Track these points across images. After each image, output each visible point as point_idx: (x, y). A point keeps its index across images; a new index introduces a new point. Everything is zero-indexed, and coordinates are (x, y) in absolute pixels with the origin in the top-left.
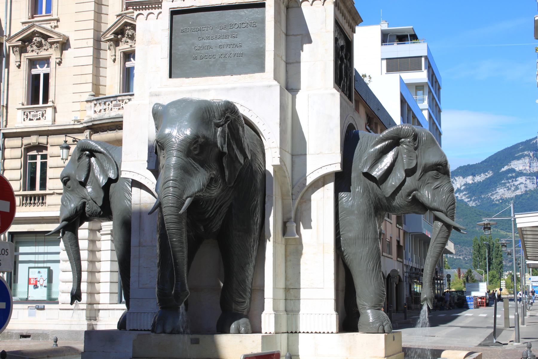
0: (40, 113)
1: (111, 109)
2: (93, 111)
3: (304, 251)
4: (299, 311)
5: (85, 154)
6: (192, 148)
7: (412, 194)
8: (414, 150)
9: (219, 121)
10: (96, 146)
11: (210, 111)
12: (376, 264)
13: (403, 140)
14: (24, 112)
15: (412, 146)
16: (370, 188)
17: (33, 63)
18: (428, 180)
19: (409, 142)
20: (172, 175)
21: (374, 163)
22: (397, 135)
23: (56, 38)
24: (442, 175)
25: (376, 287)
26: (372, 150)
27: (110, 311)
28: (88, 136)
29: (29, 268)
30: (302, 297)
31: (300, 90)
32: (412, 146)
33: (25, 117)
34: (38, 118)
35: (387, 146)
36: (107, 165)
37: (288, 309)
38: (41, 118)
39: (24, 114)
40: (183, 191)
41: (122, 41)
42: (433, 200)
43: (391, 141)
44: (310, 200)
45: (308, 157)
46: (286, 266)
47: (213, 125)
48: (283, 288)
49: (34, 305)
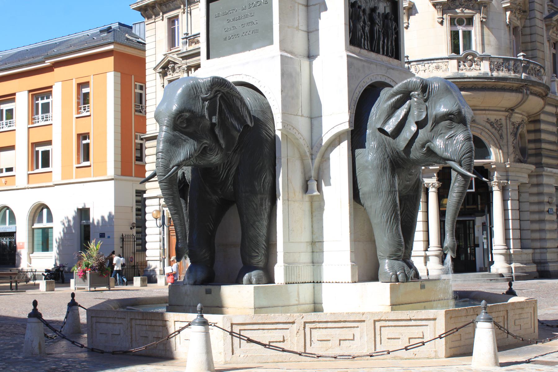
4: (323, 262)
6: (178, 122)
7: (426, 146)
8: (423, 102)
9: (206, 96)
11: (197, 87)
12: (390, 216)
13: (413, 93)
15: (421, 98)
16: (385, 142)
18: (441, 131)
19: (418, 95)
21: (387, 118)
22: (406, 89)
24: (456, 124)
25: (390, 239)
30: (325, 249)
31: (318, 57)
32: (421, 98)
37: (315, 261)
43: (402, 95)
44: (329, 159)
46: (312, 222)
47: (201, 100)
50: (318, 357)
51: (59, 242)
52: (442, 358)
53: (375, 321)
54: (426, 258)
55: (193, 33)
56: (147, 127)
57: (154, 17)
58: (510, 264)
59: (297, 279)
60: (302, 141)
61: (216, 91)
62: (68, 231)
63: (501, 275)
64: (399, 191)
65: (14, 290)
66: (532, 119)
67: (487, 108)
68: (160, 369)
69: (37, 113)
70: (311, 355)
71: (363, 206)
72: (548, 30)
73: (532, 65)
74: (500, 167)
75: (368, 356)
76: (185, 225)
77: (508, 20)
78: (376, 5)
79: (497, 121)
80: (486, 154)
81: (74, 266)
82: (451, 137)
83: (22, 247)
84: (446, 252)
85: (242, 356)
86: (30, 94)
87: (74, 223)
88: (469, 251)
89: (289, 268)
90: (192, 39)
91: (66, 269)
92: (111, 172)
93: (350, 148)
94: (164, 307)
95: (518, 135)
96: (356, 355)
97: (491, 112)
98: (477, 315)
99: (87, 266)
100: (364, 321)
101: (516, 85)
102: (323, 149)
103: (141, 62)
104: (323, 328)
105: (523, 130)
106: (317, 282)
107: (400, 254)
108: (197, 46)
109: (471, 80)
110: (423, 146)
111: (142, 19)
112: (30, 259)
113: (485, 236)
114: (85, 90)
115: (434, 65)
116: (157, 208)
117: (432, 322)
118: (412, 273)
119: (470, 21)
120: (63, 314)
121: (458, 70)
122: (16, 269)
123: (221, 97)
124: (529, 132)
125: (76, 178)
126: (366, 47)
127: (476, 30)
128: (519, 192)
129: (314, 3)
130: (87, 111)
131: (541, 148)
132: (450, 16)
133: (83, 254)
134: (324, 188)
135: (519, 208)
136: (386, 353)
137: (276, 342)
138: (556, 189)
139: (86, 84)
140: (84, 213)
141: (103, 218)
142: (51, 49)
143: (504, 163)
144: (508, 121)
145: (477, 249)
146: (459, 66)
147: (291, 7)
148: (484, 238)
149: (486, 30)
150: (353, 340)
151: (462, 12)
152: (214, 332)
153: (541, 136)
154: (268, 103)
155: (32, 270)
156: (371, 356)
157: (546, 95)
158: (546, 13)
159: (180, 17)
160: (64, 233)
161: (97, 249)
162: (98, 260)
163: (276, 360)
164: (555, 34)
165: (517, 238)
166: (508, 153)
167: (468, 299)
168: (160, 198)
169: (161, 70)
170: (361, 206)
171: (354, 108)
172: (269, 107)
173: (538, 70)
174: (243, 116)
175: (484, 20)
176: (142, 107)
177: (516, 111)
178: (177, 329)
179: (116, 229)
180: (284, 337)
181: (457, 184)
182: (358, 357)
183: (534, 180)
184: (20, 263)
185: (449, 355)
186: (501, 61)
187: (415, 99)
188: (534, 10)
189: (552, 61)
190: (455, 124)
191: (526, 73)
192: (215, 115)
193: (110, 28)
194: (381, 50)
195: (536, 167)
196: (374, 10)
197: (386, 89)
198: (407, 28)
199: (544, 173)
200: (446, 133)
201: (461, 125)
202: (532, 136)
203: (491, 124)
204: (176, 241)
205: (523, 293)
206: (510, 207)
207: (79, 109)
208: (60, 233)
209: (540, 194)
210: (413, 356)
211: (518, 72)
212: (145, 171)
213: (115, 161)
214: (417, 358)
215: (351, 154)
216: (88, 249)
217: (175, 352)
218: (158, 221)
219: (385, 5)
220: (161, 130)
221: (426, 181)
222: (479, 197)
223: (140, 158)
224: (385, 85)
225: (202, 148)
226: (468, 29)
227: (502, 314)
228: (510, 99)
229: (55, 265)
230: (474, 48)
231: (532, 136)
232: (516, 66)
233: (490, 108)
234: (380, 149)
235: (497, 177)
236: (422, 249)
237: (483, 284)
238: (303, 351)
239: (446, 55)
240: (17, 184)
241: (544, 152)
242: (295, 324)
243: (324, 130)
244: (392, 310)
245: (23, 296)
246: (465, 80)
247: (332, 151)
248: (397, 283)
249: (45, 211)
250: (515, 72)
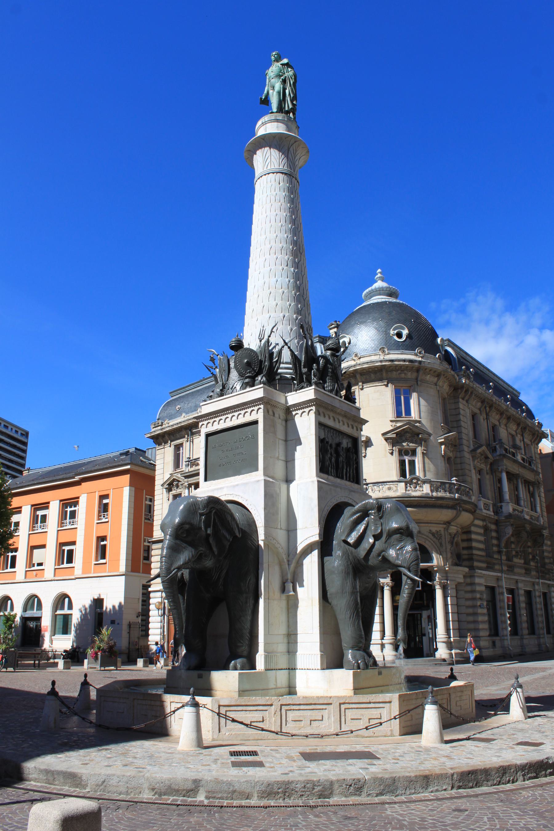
3: (300, 604)
4: (297, 652)
6: (180, 533)
8: (379, 519)
13: (370, 511)
16: (348, 551)
18: (393, 542)
19: (375, 513)
24: (405, 537)
26: (348, 522)
35: (358, 517)
40: (171, 565)
42: (397, 558)
44: (302, 564)
45: (298, 531)
46: (288, 617)
47: (198, 515)
48: (284, 634)
50: (292, 736)
51: (77, 627)
52: (396, 736)
53: (340, 704)
54: (383, 646)
55: (194, 458)
56: (154, 532)
58: (451, 650)
59: (275, 666)
60: (280, 550)
61: (212, 508)
62: (84, 617)
63: (444, 660)
64: (360, 592)
65: (36, 668)
66: (465, 530)
67: (429, 522)
68: (156, 745)
69: (66, 519)
70: (287, 734)
71: (330, 604)
72: (474, 460)
73: (463, 488)
74: (441, 570)
75: (334, 734)
76: (182, 618)
77: (443, 452)
78: (340, 441)
79: (437, 532)
80: (430, 559)
81: (88, 648)
82: (401, 548)
83: (46, 631)
84: (398, 644)
85: (227, 734)
86: (61, 503)
87: (90, 611)
88: (417, 639)
89: (268, 657)
90: (193, 462)
91: (81, 650)
92: (122, 568)
93: (320, 556)
94: (161, 688)
95: (454, 543)
96: (324, 734)
97: (432, 525)
98: (426, 698)
99: (99, 648)
100: (331, 704)
101: (451, 503)
102: (297, 556)
103: (151, 480)
104: (296, 710)
105: (458, 539)
106: (292, 669)
107: (361, 645)
108: (197, 468)
109: (416, 499)
110: (379, 555)
111: (154, 445)
112: (51, 641)
113: (430, 627)
114: (105, 501)
115: (387, 486)
116: (160, 600)
117: (388, 704)
118: (371, 661)
119: (414, 453)
120: (77, 691)
121: (406, 490)
122: (39, 648)
123: (215, 512)
124: (463, 540)
125: (94, 573)
126: (333, 474)
128: (456, 590)
129: (291, 439)
130: (106, 518)
131: (472, 554)
132: (399, 448)
133: (96, 638)
134: (299, 589)
135: (457, 603)
136: (350, 732)
137: (257, 722)
138: (486, 587)
139: (107, 496)
140: (98, 602)
141: (114, 607)
142: (80, 467)
143: (444, 566)
144: (446, 532)
145: (424, 638)
146: (406, 488)
147: (273, 441)
148: (430, 629)
149: (427, 460)
150: (322, 720)
151: (408, 445)
152: (204, 712)
153: (472, 544)
154: (253, 518)
155: (52, 650)
156: (337, 735)
157: (475, 511)
158: (472, 447)
159: (184, 444)
160: (81, 619)
161: (108, 635)
162: (109, 643)
163: (256, 738)
164: (479, 464)
165: (456, 628)
166: (447, 558)
167: (417, 683)
168: (162, 592)
169: (167, 486)
170: (328, 604)
171: (323, 523)
172: (254, 522)
173: (468, 492)
174: (233, 528)
175: (425, 452)
176: (150, 515)
177: (452, 524)
178: (173, 709)
179: (125, 616)
180: (263, 718)
181: (407, 587)
182: (326, 735)
183: (468, 580)
184: (43, 643)
185: (402, 733)
186: (439, 484)
187: (372, 517)
188: (465, 475)
189: (478, 484)
190: (404, 537)
191: (458, 494)
192: (210, 527)
193: (128, 451)
194: (345, 477)
195: (469, 570)
196: (338, 445)
197: (349, 508)
198: (365, 457)
199: (475, 574)
200: (397, 545)
201: (409, 538)
202: (465, 544)
203: (433, 534)
204: (174, 632)
205: (462, 675)
206: (449, 603)
207: (99, 516)
208: (78, 619)
209: (473, 591)
210: (372, 734)
211: (452, 493)
212: (151, 569)
213: (127, 560)
214: (376, 737)
215: (320, 561)
216: (100, 634)
217: (170, 729)
218: (160, 611)
219: (348, 441)
220: (165, 536)
221: (382, 580)
222: (425, 594)
223: (148, 558)
224: (347, 505)
225: (199, 554)
226: (413, 458)
227: (446, 696)
228: (446, 514)
229: (72, 646)
230: (417, 474)
231: (465, 544)
232: (450, 488)
233: (432, 522)
234: (344, 557)
235: (438, 578)
236: (379, 638)
237: (430, 667)
238: (280, 731)
239: (395, 478)
240: (45, 577)
241: (475, 557)
242: (273, 706)
243: (299, 541)
244: (354, 694)
245: (44, 673)
246: (412, 499)
247: (305, 558)
248: (359, 670)
249: (67, 600)
250: (450, 493)
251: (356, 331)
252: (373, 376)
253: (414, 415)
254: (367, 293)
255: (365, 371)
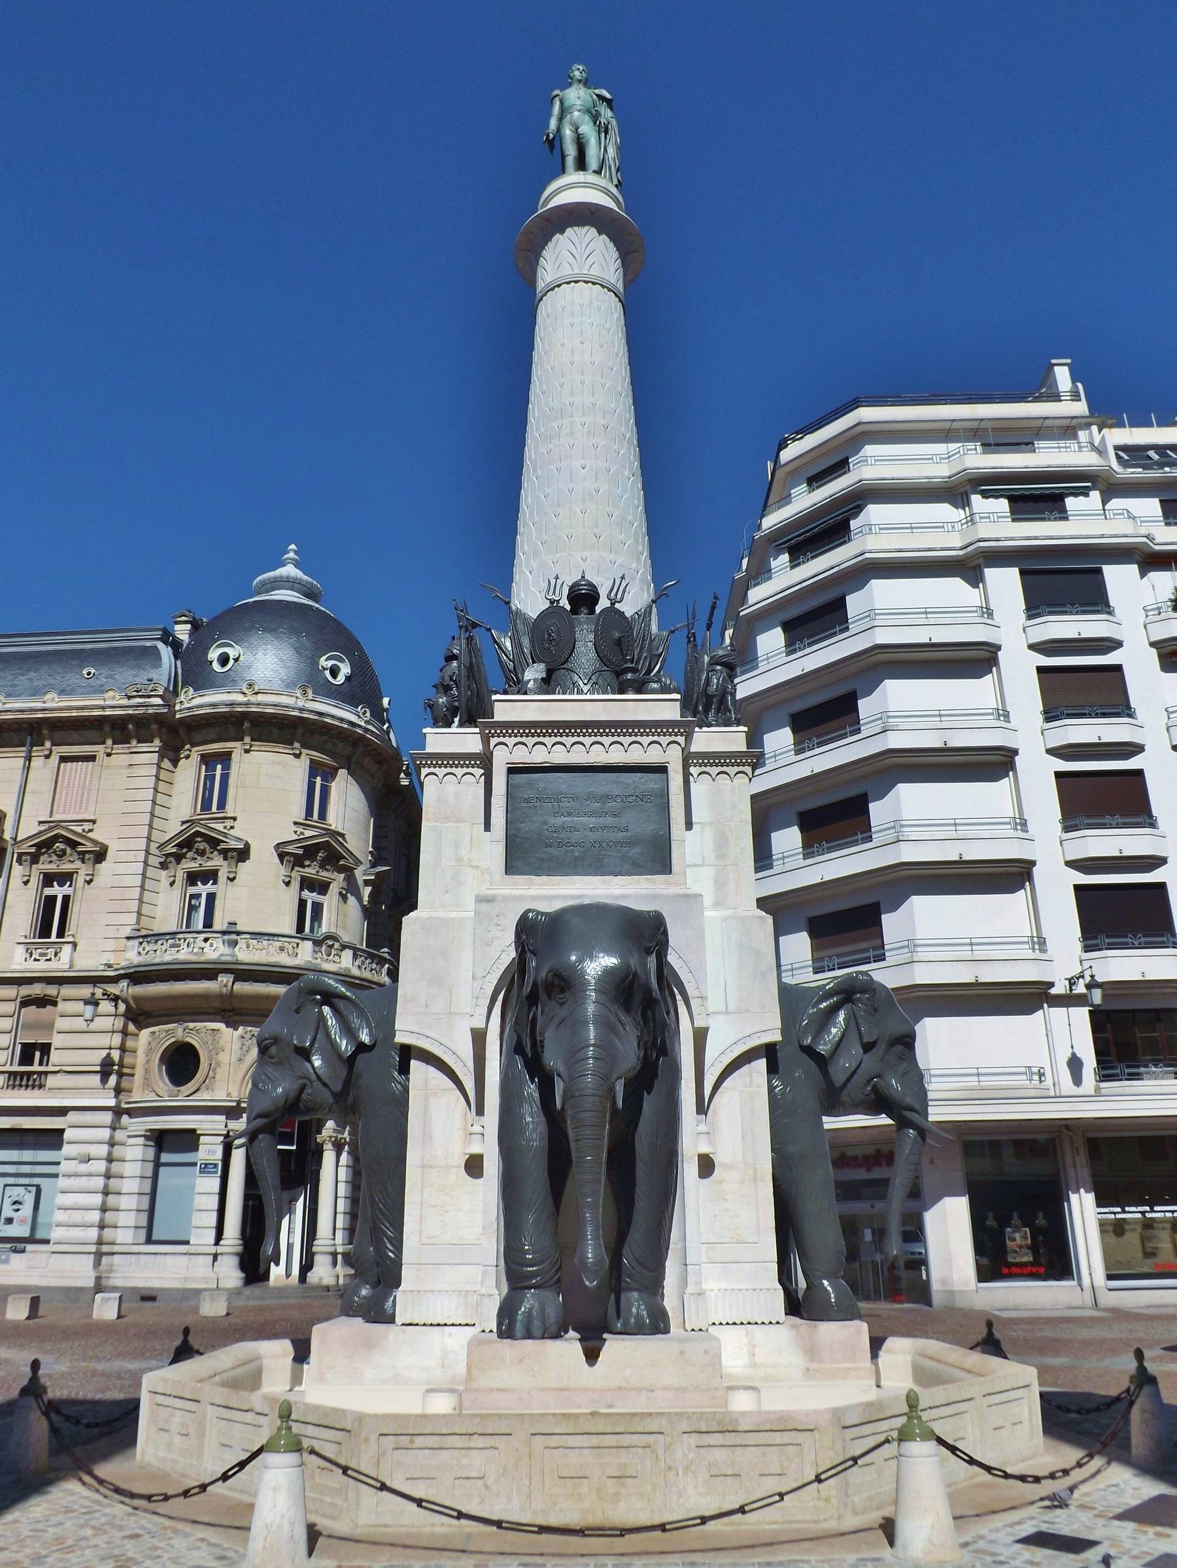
0: (51, 951)
1: (166, 950)
2: (135, 952)
5: (314, 999)
7: (872, 1083)
10: (337, 987)
14: (28, 949)
17: (49, 879)
20: (592, 1035)
23: (90, 847)
27: (133, 1256)
28: (125, 987)
29: (6, 1186)
33: (28, 955)
34: (48, 958)
36: (356, 1020)
38: (53, 958)
39: (27, 951)
41: (187, 856)
49: (9, 1246)
57: (109, 742)
115: (278, 944)
127: (329, 902)
136: (350, 1472)
175: (344, 892)
251: (254, 640)
252: (275, 731)
253: (335, 819)
254: (269, 579)
255: (263, 720)
